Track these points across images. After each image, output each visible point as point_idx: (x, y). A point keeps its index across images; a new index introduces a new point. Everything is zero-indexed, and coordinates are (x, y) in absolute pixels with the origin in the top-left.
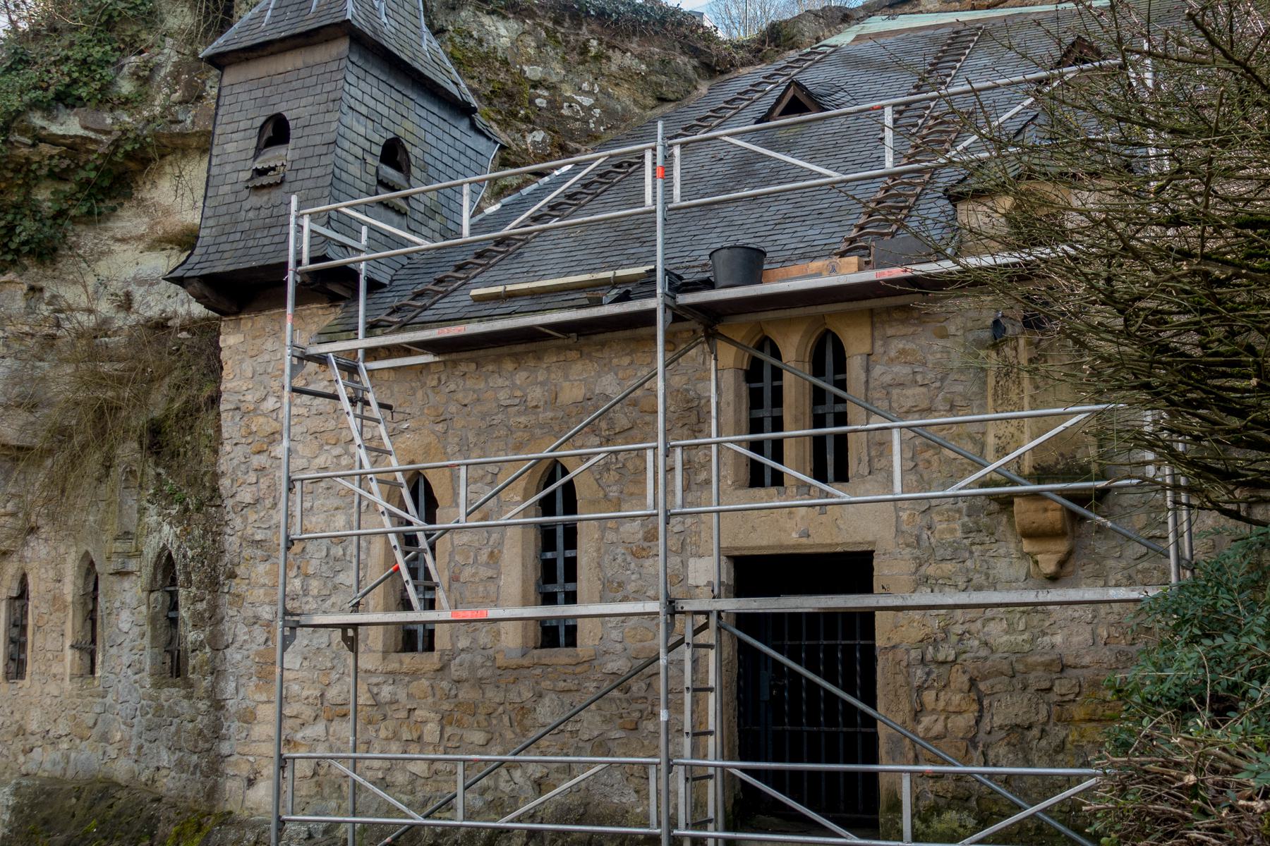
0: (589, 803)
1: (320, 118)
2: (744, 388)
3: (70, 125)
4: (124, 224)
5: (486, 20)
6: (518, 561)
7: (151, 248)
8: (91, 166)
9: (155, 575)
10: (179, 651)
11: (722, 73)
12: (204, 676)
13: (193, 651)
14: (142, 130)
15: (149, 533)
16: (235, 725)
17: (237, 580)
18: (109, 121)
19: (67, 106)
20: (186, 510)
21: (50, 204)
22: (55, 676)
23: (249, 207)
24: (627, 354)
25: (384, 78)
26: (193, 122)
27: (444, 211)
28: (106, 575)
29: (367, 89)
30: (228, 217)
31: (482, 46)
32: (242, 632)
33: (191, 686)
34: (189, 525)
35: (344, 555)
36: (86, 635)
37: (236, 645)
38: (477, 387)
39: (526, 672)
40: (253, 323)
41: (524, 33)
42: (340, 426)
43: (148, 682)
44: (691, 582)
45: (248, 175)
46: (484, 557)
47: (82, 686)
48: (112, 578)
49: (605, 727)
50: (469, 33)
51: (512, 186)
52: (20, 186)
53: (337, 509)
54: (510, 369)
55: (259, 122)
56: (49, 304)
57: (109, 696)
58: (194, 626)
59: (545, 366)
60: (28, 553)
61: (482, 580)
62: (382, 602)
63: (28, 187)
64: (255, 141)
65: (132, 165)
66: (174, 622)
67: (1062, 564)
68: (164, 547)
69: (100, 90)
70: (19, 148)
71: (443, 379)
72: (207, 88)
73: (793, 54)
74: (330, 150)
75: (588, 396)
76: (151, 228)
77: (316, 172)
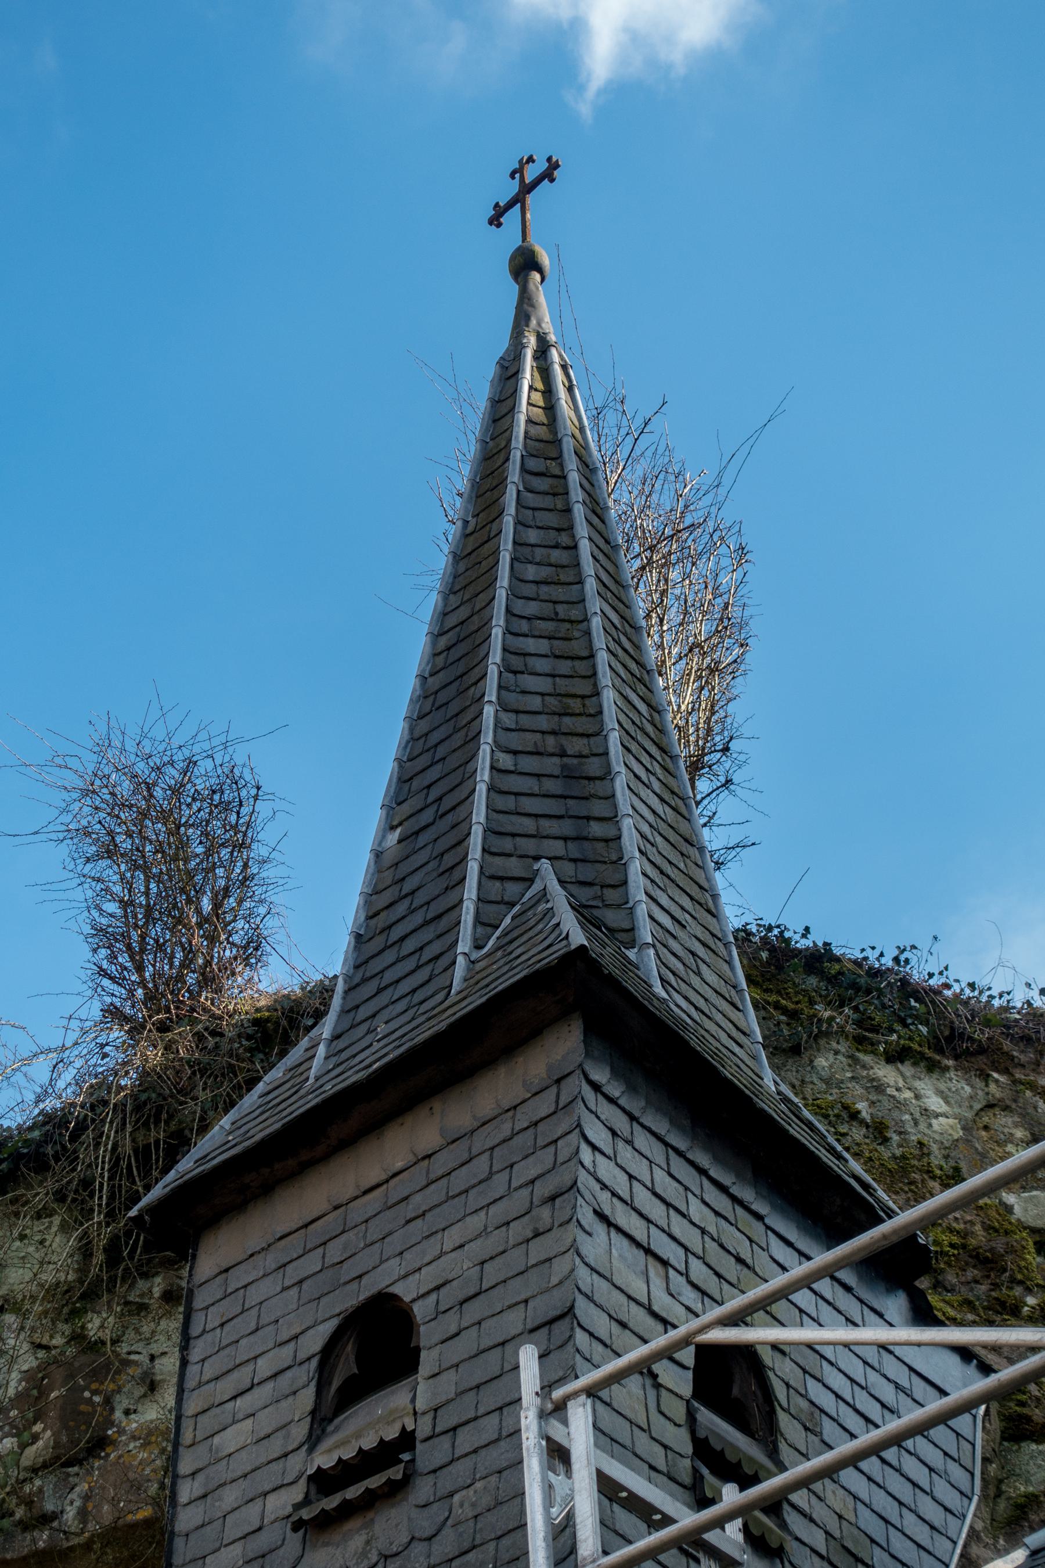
5: (886, 1074)
25: (681, 1144)
26: (83, 1514)
31: (886, 1140)
41: (990, 1106)
45: (297, 1493)
50: (846, 1107)
55: (315, 1341)
64: (307, 1398)
72: (118, 1414)
74: (557, 1341)
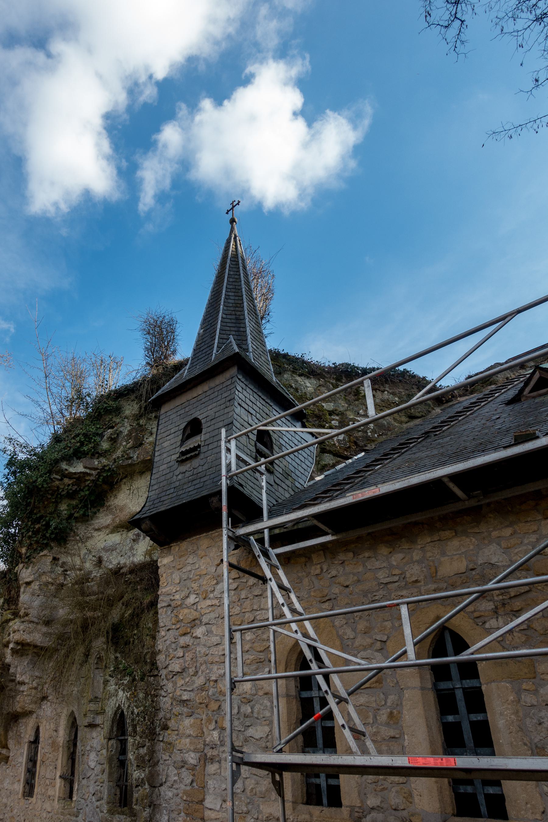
3: (78, 468)
4: (100, 521)
5: (299, 379)
6: (422, 721)
7: (112, 532)
8: (87, 488)
9: (112, 727)
10: (126, 786)
11: (447, 402)
12: (144, 808)
13: (137, 786)
14: (112, 466)
15: (110, 697)
17: (169, 732)
18: (96, 463)
19: (77, 459)
20: (134, 680)
21: (66, 512)
22: (49, 797)
23: (178, 473)
24: (507, 526)
26: (137, 457)
27: (293, 475)
28: (82, 727)
29: (247, 395)
30: (165, 482)
31: (298, 392)
32: (172, 771)
33: (135, 815)
34: (135, 690)
35: (252, 712)
36: (68, 769)
37: (168, 784)
38: (355, 571)
40: (180, 547)
41: (320, 386)
42: (243, 611)
43: (105, 808)
46: (383, 717)
47: (64, 806)
48: (86, 729)
51: (329, 464)
52: (53, 502)
54: (385, 553)
55: (182, 426)
56: (61, 567)
57: (80, 816)
58: (137, 766)
59: (419, 547)
60: (41, 713)
63: (57, 503)
65: (105, 487)
66: (122, 764)
68: (119, 707)
69: (93, 448)
70: (55, 481)
71: (325, 567)
72: (145, 439)
73: (493, 387)
75: (471, 566)
76: (113, 520)
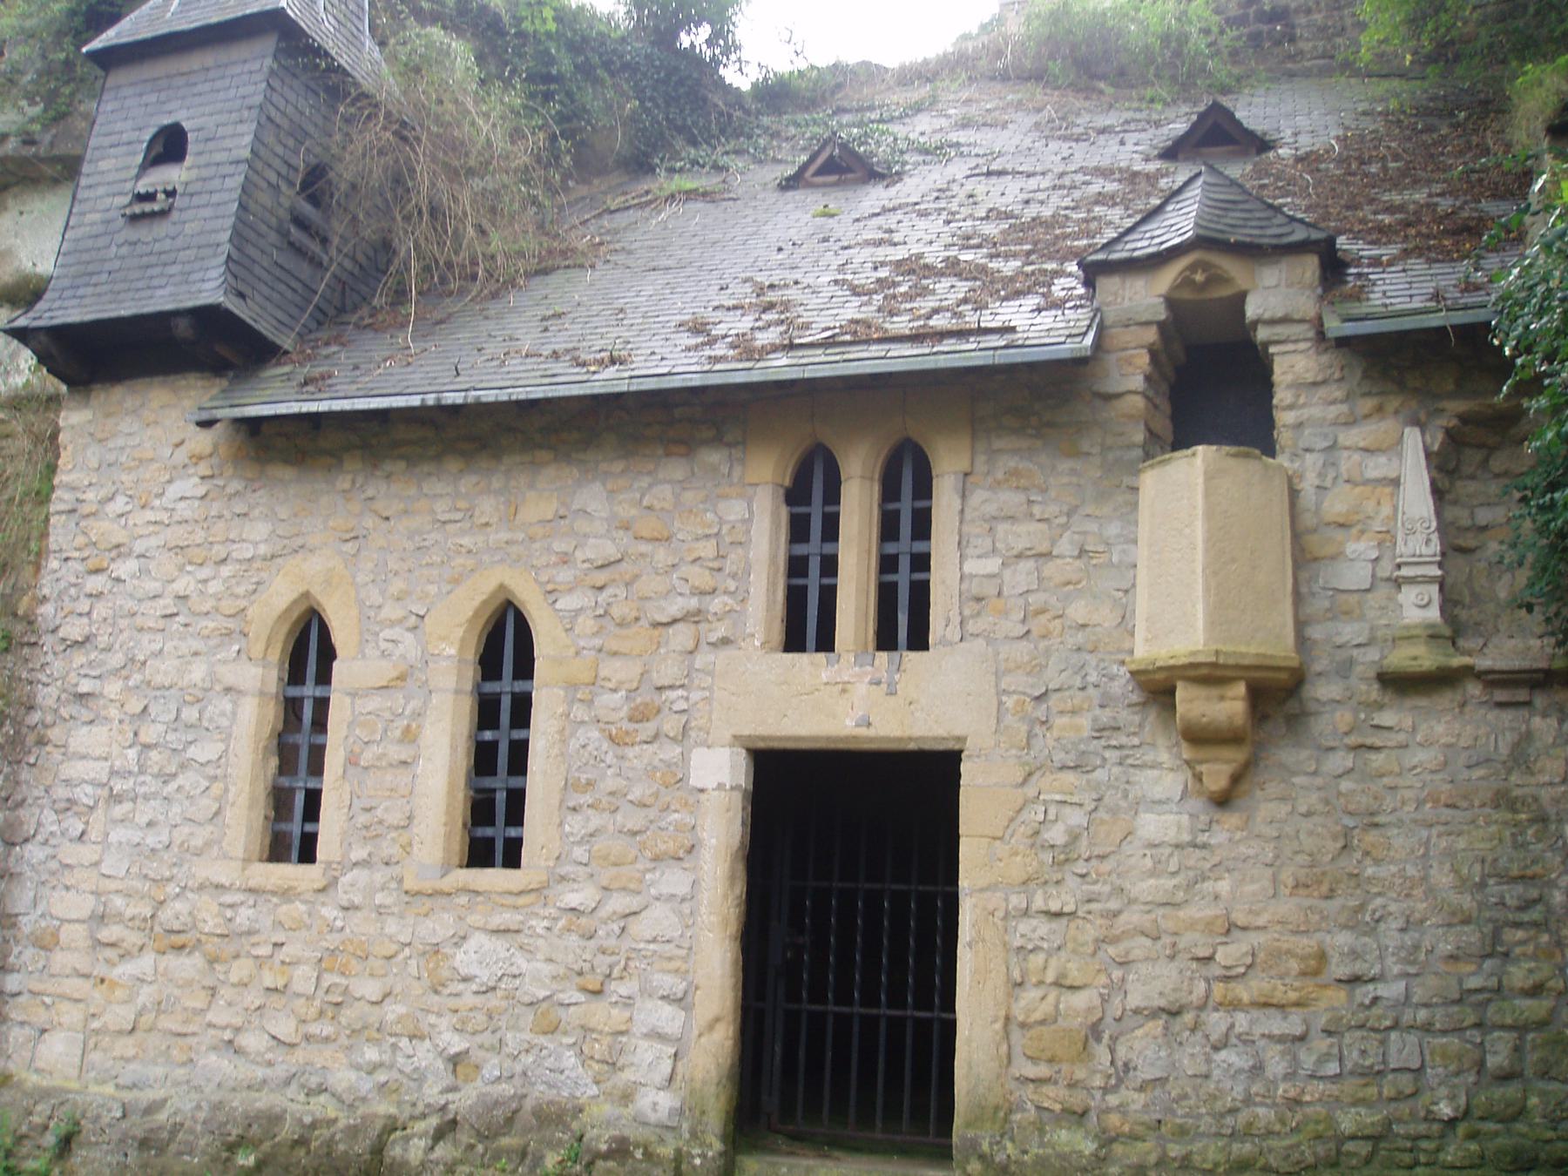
0: (525, 1096)
1: (229, 130)
2: (784, 512)
16: (29, 952)
17: (49, 748)
29: (292, 97)
37: (39, 838)
39: (443, 901)
44: (694, 781)
49: (555, 986)
53: (196, 654)
61: (391, 765)
62: (247, 788)
64: (140, 159)
67: (1236, 779)
77: (216, 198)
